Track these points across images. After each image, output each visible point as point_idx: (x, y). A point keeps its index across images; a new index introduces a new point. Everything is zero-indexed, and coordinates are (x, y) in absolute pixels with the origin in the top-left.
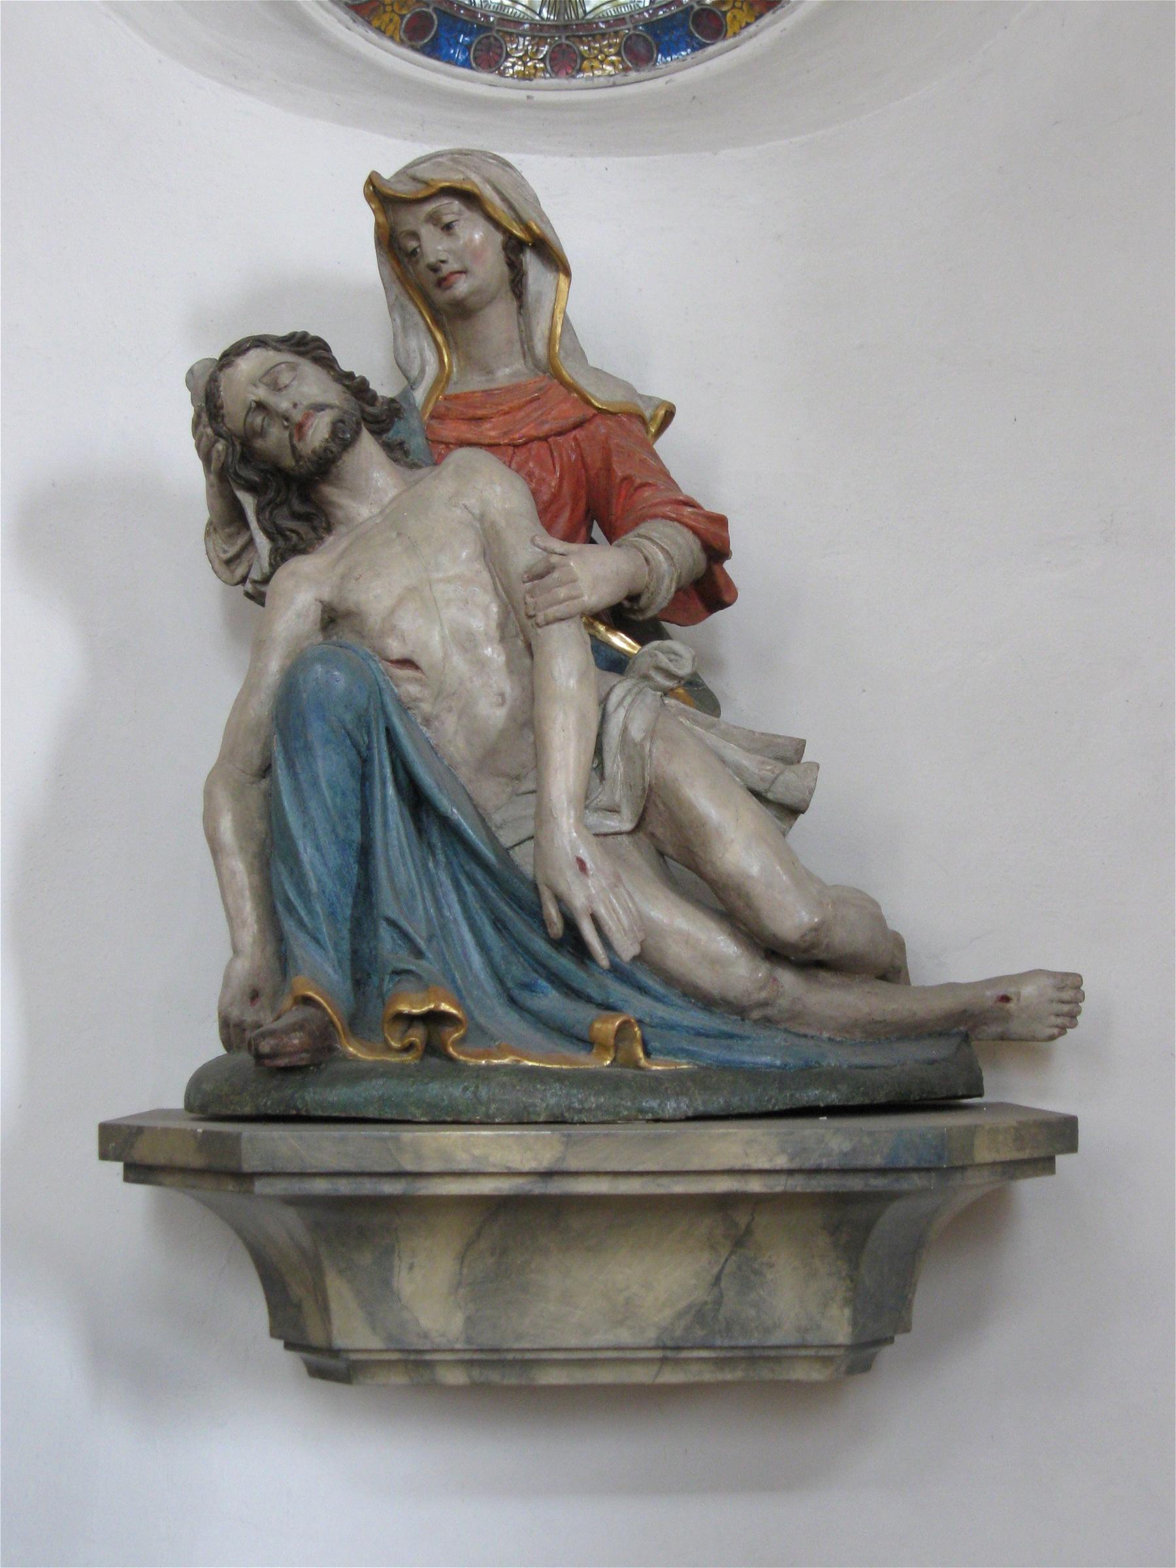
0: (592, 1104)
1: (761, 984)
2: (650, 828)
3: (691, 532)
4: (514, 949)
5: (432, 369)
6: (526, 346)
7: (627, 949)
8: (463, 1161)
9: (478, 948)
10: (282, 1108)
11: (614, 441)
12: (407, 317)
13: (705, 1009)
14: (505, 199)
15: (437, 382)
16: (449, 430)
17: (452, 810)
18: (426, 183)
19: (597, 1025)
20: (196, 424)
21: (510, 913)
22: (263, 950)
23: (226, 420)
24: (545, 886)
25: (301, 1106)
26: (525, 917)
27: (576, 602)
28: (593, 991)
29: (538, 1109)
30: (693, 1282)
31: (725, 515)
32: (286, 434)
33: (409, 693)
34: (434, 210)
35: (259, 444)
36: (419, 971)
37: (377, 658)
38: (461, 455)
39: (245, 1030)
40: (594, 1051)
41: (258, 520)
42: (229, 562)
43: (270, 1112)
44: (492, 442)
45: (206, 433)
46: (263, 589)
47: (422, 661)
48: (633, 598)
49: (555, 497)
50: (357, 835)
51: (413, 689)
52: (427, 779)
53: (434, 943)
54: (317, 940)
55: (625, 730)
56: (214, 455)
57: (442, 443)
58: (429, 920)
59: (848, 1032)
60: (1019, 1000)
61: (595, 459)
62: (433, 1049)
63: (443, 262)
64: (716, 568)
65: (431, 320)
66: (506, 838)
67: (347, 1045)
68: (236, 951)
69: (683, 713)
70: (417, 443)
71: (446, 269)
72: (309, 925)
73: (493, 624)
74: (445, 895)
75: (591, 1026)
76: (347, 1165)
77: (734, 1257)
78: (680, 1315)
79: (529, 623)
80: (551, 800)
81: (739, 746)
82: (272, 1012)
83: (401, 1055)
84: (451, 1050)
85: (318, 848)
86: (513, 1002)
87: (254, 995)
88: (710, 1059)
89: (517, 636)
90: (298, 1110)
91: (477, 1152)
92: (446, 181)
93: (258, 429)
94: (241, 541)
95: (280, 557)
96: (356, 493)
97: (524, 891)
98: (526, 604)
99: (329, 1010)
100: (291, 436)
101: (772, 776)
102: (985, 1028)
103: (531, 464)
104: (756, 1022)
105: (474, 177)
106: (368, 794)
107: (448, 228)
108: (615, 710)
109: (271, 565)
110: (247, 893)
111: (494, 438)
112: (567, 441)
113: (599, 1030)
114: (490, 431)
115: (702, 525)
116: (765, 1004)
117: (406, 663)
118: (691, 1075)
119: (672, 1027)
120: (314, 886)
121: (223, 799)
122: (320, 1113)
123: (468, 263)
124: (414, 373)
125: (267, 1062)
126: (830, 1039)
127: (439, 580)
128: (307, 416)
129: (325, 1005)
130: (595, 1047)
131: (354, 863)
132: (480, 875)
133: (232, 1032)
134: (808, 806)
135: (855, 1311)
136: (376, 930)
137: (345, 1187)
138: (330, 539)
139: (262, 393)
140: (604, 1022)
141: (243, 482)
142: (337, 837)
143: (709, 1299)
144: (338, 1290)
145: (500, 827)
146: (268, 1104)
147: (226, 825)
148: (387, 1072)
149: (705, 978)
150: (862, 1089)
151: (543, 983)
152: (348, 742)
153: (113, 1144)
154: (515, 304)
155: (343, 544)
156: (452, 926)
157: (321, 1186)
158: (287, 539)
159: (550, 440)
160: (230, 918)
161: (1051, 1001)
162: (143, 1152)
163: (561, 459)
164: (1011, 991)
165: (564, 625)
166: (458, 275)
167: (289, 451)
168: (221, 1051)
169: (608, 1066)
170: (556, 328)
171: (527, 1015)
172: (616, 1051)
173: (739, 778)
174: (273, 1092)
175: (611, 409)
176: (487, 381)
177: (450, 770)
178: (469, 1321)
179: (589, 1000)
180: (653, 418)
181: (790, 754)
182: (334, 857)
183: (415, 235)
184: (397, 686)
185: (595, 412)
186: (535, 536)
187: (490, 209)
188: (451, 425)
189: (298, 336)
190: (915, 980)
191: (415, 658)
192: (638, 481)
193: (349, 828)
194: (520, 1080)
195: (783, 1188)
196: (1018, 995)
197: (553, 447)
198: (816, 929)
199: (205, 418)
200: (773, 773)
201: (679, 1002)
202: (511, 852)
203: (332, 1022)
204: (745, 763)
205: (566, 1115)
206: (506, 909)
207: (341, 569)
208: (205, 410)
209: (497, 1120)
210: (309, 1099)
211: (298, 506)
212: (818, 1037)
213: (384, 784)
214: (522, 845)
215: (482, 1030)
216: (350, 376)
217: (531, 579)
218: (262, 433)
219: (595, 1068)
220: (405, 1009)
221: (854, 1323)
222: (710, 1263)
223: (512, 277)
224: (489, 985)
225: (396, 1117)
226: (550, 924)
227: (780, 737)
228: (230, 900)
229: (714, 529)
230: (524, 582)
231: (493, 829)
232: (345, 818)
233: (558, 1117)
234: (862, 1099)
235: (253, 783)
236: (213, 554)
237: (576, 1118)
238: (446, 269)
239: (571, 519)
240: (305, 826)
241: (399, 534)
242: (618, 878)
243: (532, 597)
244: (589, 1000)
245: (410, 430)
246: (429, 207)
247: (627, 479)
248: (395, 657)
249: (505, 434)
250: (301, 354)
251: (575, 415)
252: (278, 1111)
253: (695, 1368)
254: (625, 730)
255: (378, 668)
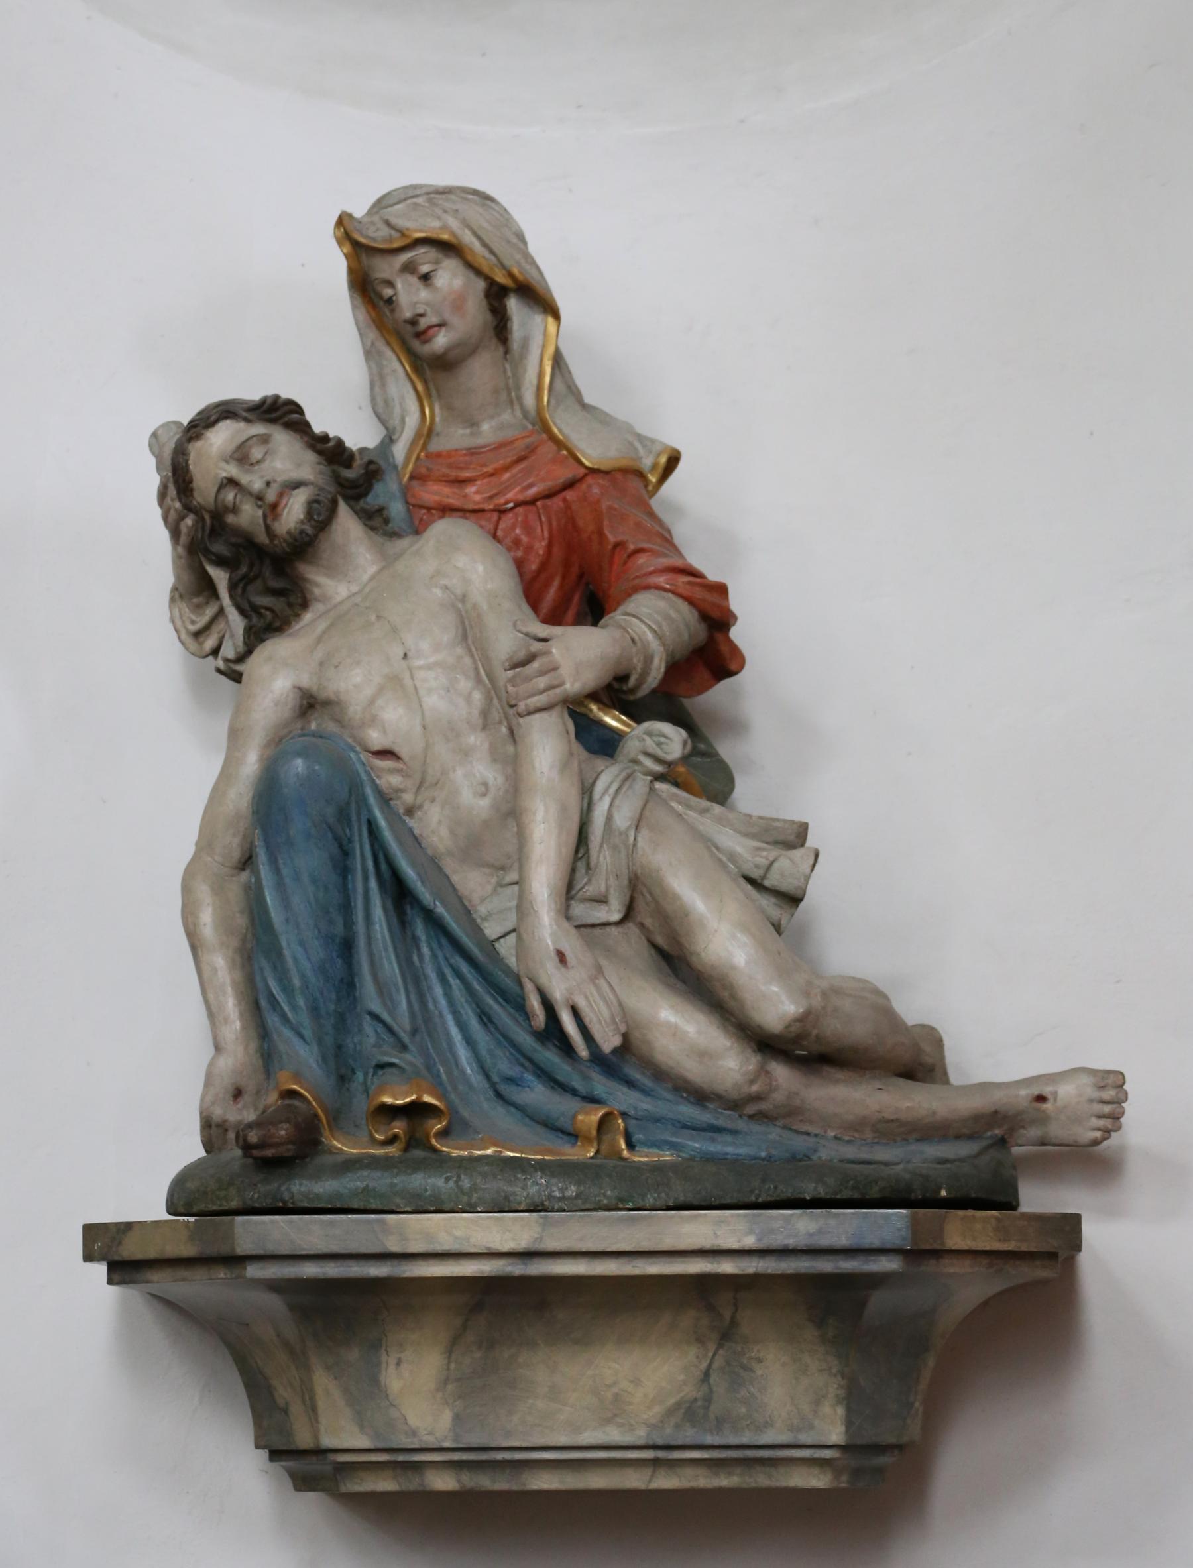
0: (573, 1193)
1: (752, 1077)
2: (639, 919)
3: (686, 603)
4: (499, 1043)
5: (412, 421)
6: (513, 394)
7: (609, 1041)
8: (445, 1243)
9: (464, 1042)
10: (269, 1201)
11: (605, 504)
12: (385, 363)
13: (698, 1104)
14: (484, 244)
15: (418, 435)
16: (434, 493)
17: (435, 903)
18: (403, 233)
19: (580, 1117)
20: (162, 496)
21: (496, 1007)
22: (246, 1048)
23: (196, 494)
24: (527, 979)
25: (287, 1198)
26: (512, 1011)
27: (558, 690)
28: (577, 1083)
29: (518, 1198)
30: (682, 1377)
31: (724, 581)
32: (260, 513)
33: (390, 784)
34: (410, 260)
35: (230, 519)
36: (402, 1064)
37: (358, 748)
38: (442, 528)
39: (226, 1130)
40: (579, 1143)
41: (232, 597)
42: (197, 634)
43: (257, 1205)
44: (476, 507)
45: (174, 507)
46: (239, 668)
47: (403, 752)
48: (622, 678)
49: (543, 566)
50: (339, 929)
51: (395, 780)
52: (409, 872)
53: (418, 1038)
54: (301, 1036)
55: (609, 818)
56: (184, 530)
57: (421, 507)
58: (412, 1015)
59: (856, 1131)
60: (1055, 1100)
61: (585, 522)
62: (414, 1141)
63: (421, 315)
64: (719, 636)
65: (410, 367)
66: (491, 930)
67: (332, 1139)
68: (218, 1048)
69: (674, 797)
70: (397, 509)
71: (423, 323)
72: (294, 1021)
73: (476, 712)
74: (430, 988)
75: (574, 1117)
76: (335, 1248)
77: (721, 1352)
78: (670, 1412)
79: (512, 712)
80: (531, 893)
81: (735, 830)
82: (255, 1111)
83: (385, 1148)
84: (434, 1142)
85: (302, 943)
86: (499, 1095)
87: (238, 1094)
88: (692, 1150)
89: (500, 722)
90: (285, 1202)
91: (458, 1233)
92: (421, 231)
93: (231, 505)
94: (210, 612)
95: (256, 636)
96: (333, 571)
97: (508, 983)
98: (507, 692)
99: (314, 1103)
100: (265, 516)
101: (767, 863)
102: (1022, 1131)
103: (518, 531)
104: (751, 1117)
105: (453, 223)
106: (350, 886)
107: (426, 278)
108: (601, 798)
109: (245, 643)
110: (229, 990)
111: (478, 503)
112: (556, 502)
113: (582, 1121)
114: (474, 494)
115: (699, 594)
116: (757, 1098)
117: (387, 753)
118: (673, 1167)
119: (658, 1120)
120: (297, 982)
121: (203, 892)
122: (306, 1205)
123: (448, 316)
124: (395, 422)
125: (255, 1153)
126: (836, 1137)
127: (420, 668)
128: (281, 495)
129: (309, 1097)
130: (579, 1139)
131: (338, 957)
132: (464, 968)
133: (213, 1132)
134: (804, 895)
135: (849, 1410)
136: (360, 1024)
137: (332, 1270)
138: (308, 617)
139: (232, 470)
140: (587, 1114)
141: (214, 558)
142: (320, 932)
143: (700, 1395)
144: (324, 1383)
145: (485, 919)
146: (254, 1196)
147: (207, 918)
148: (374, 1163)
149: (692, 1070)
150: (851, 1182)
151: (528, 1077)
152: (330, 835)
153: (99, 1244)
154: (501, 350)
155: (322, 626)
156: (437, 1020)
157: (310, 1270)
158: (260, 615)
159: (539, 503)
160: (211, 1015)
161: (1091, 1101)
162: (131, 1249)
163: (550, 524)
164: (1047, 1090)
165: (545, 715)
166: (436, 329)
167: (263, 529)
168: (203, 1153)
169: (591, 1158)
170: (544, 377)
171: (513, 1110)
172: (599, 1144)
173: (733, 865)
174: (259, 1185)
175: (603, 467)
176: (472, 434)
177: (435, 863)
178: (457, 1418)
179: (574, 1092)
180: (654, 466)
181: (792, 838)
182: (318, 951)
183: (390, 284)
184: (378, 777)
185: (587, 471)
186: (517, 620)
187: (469, 258)
188: (434, 487)
189: (269, 401)
190: (955, 1078)
191: (396, 749)
192: (632, 547)
193: (331, 922)
194: (501, 1170)
195: (754, 1270)
196: (1055, 1094)
197: (541, 511)
198: (801, 1019)
199: (172, 491)
200: (767, 859)
201: (670, 1096)
202: (497, 945)
203: (316, 1116)
204: (739, 849)
205: (547, 1203)
206: (491, 1002)
207: (319, 654)
208: (171, 480)
209: (479, 1210)
210: (295, 1192)
211: (275, 584)
212: (822, 1136)
213: (366, 879)
214: (507, 938)
215: (466, 1125)
216: (325, 438)
217: (515, 666)
218: (235, 510)
219: (578, 1159)
220: (388, 1100)
221: (849, 1423)
222: (697, 1357)
223: (495, 323)
224: (476, 1079)
225: (380, 1207)
226: (533, 1017)
227: (778, 820)
228: (211, 996)
229: (711, 598)
230: (506, 670)
231: (479, 920)
232: (328, 912)
233: (538, 1206)
234: (851, 1193)
235: (232, 876)
236: (179, 623)
237: (556, 1207)
238: (423, 323)
239: (561, 587)
240: (287, 920)
241: (379, 617)
242: (600, 970)
243: (514, 686)
244: (574, 1092)
245: (387, 493)
246: (405, 257)
247: (619, 545)
248: (376, 748)
249: (491, 498)
250: (273, 421)
251: (565, 473)
252: (264, 1204)
253: (689, 1471)
254: (609, 818)
255: (359, 758)
